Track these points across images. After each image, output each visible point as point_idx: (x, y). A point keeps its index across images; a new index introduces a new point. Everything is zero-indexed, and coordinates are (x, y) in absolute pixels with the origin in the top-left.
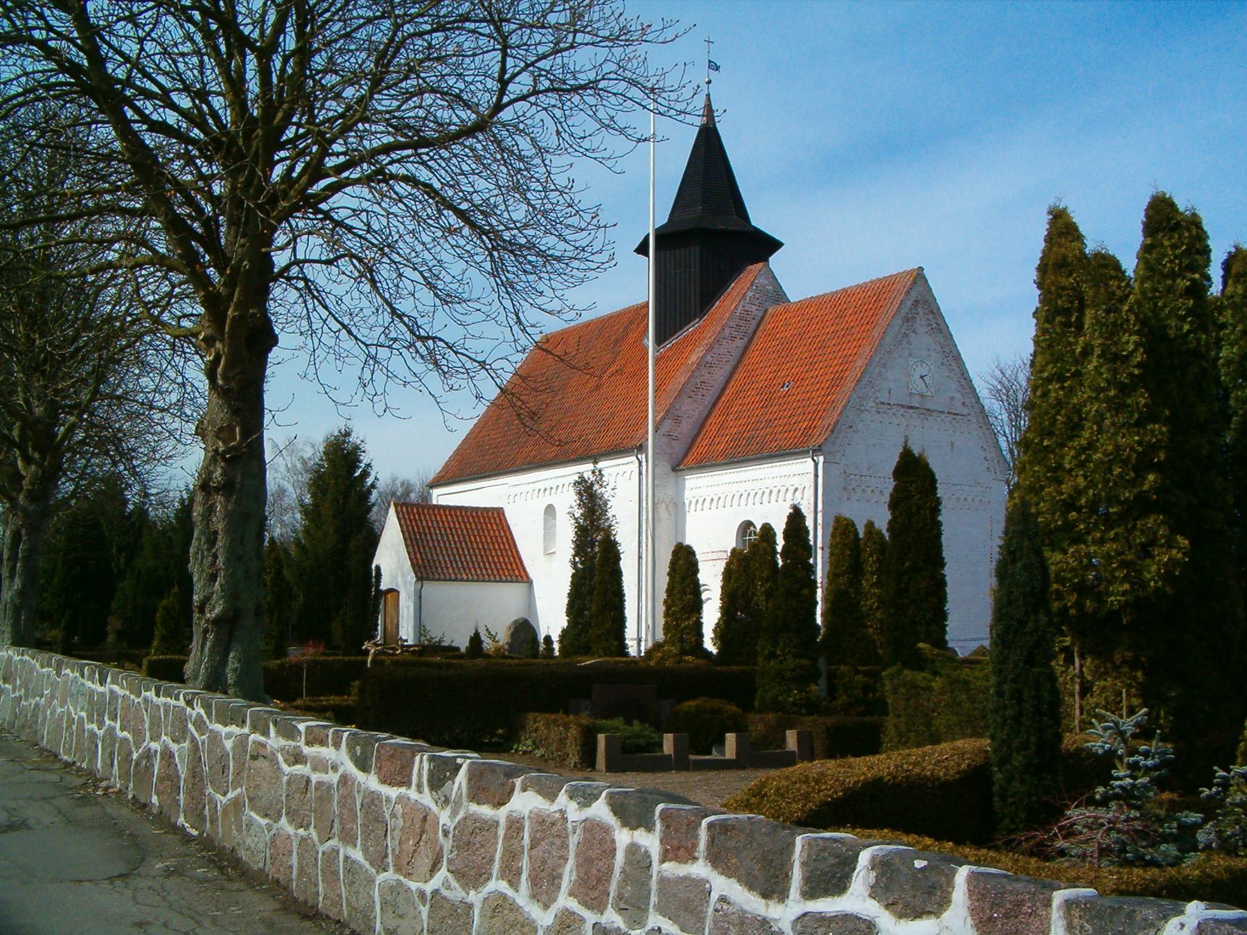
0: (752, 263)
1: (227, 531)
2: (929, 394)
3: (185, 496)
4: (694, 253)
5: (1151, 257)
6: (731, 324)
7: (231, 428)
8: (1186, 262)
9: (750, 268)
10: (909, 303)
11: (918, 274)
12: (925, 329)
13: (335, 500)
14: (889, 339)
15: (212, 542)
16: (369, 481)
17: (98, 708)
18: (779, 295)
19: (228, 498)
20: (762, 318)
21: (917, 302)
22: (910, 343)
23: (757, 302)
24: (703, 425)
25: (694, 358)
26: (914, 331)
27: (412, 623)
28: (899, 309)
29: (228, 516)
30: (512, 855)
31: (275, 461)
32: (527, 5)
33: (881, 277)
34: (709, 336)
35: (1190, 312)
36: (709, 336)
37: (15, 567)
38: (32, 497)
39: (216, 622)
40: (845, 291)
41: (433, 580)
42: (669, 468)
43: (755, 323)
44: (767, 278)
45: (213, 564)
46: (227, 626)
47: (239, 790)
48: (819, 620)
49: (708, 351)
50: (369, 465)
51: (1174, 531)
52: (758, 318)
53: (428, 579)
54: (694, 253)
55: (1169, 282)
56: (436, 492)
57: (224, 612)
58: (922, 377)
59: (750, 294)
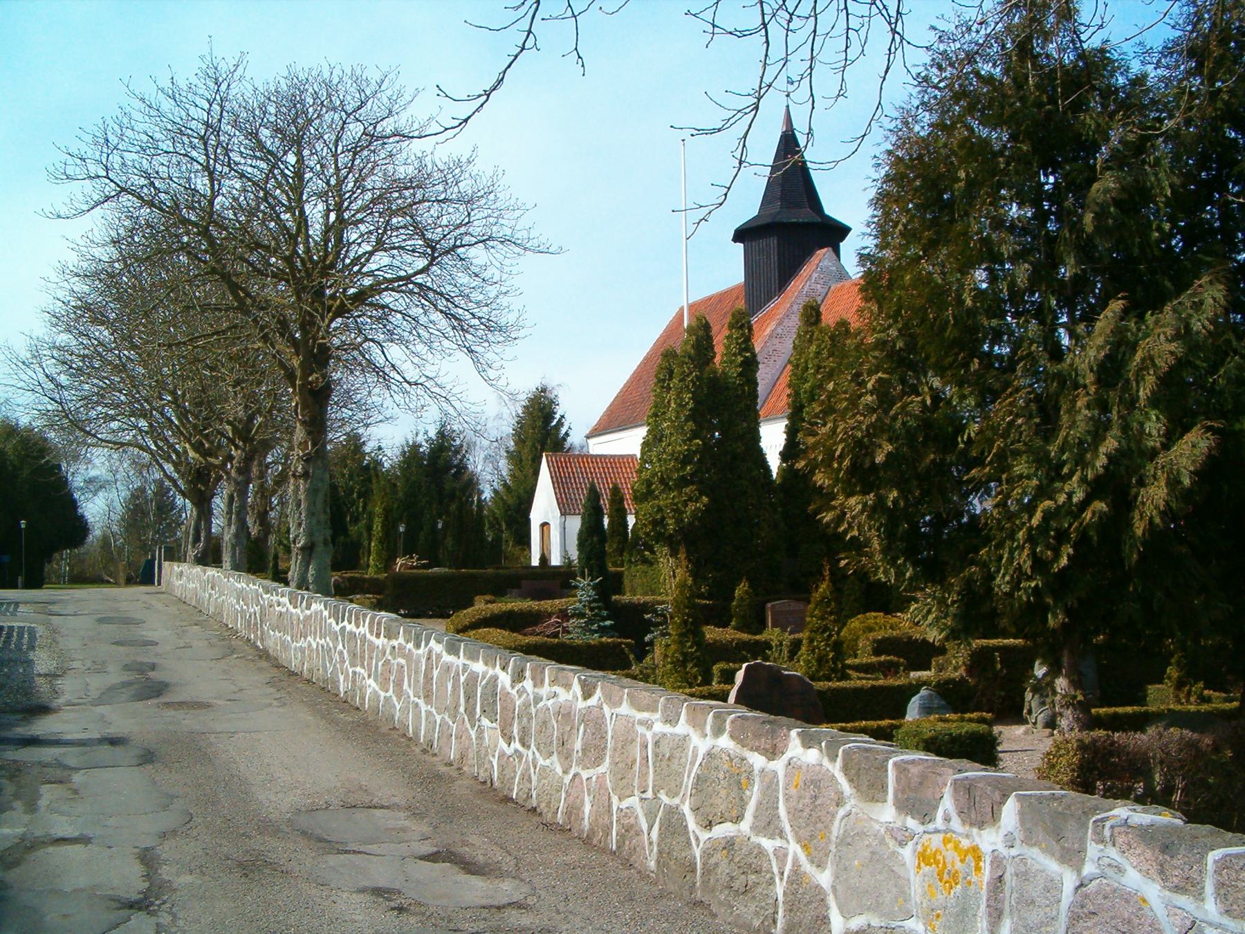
1: (306, 499)
3: (406, 449)
4: (773, 242)
6: (799, 301)
7: (306, 442)
8: (743, 346)
9: (819, 252)
15: (299, 505)
16: (563, 430)
17: (240, 595)
19: (306, 481)
23: (821, 282)
24: (775, 384)
25: (768, 331)
29: (307, 491)
34: (782, 311)
36: (782, 311)
37: (231, 518)
38: (240, 471)
39: (302, 549)
45: (300, 517)
46: (308, 550)
49: (779, 324)
50: (563, 417)
52: (823, 295)
53: (570, 514)
54: (773, 242)
56: (592, 441)
57: (305, 544)
59: (815, 275)
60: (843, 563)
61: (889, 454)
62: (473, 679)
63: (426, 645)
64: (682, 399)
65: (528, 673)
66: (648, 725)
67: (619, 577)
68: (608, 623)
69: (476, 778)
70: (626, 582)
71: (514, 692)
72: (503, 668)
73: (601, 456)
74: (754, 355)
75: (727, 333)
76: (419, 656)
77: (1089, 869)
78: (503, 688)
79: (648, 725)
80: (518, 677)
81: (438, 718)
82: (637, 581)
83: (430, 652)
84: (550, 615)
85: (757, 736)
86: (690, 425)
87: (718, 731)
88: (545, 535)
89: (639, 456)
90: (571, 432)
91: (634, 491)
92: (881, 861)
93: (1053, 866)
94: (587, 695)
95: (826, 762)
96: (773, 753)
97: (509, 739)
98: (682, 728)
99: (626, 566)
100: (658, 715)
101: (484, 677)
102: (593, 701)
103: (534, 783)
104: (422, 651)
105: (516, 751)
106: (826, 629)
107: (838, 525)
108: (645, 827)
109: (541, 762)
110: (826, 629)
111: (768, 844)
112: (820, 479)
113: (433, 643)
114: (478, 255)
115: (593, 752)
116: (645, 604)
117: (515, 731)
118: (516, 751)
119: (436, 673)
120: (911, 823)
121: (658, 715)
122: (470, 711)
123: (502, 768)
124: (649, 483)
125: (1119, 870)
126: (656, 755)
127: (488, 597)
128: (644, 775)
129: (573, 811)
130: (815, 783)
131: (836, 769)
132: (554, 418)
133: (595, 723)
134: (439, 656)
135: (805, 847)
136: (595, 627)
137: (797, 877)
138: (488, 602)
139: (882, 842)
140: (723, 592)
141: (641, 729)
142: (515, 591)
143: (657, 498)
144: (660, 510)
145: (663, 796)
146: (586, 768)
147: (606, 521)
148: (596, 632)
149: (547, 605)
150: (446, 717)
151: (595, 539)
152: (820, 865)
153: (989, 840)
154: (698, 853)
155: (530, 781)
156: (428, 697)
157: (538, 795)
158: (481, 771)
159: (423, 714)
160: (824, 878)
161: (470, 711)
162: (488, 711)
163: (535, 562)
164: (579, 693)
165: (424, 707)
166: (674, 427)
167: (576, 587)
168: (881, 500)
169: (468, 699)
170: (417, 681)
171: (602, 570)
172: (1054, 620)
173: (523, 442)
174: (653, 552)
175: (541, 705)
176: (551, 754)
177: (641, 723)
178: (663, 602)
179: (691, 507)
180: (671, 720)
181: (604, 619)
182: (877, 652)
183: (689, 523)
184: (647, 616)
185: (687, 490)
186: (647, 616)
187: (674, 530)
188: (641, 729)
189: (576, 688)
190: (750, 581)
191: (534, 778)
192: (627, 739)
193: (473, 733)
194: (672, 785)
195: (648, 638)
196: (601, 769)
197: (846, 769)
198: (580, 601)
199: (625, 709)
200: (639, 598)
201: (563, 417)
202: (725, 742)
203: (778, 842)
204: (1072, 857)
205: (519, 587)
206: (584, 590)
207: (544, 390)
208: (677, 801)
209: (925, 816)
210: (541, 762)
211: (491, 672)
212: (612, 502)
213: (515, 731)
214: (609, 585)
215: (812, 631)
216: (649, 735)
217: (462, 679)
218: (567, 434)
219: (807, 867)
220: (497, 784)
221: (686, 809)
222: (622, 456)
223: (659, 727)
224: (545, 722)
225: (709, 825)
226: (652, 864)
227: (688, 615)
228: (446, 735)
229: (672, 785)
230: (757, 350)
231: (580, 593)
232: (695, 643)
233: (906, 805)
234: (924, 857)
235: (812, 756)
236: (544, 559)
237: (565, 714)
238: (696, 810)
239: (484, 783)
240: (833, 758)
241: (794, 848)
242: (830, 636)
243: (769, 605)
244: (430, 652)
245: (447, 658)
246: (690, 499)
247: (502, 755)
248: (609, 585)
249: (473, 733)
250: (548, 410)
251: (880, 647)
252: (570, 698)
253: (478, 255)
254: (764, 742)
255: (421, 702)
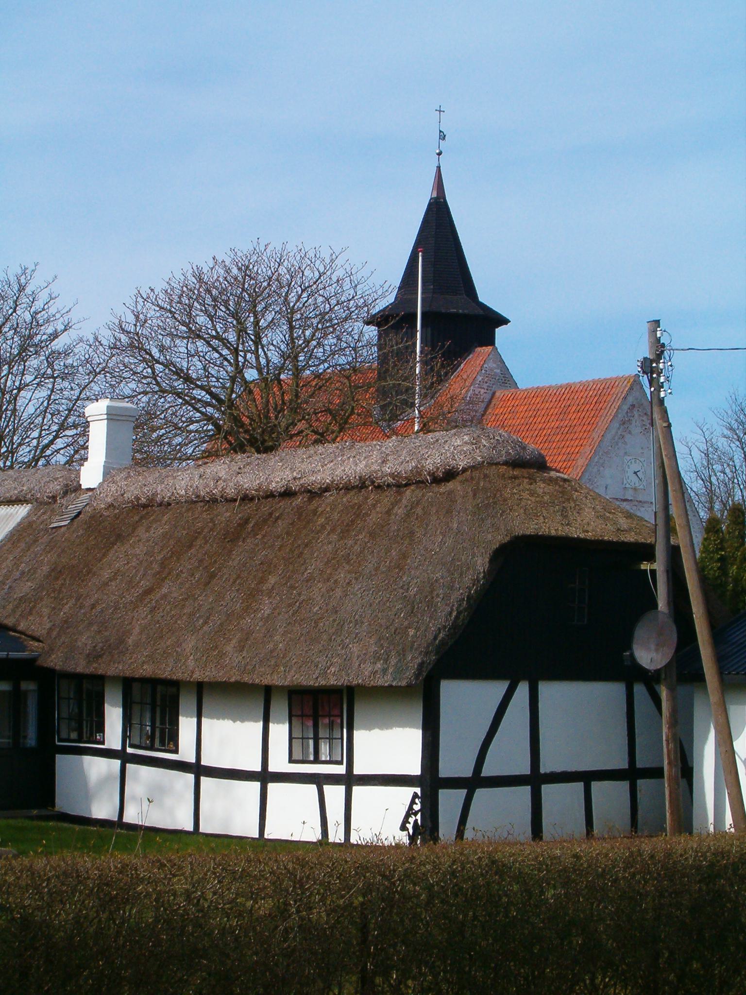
0: (481, 345)
2: (641, 487)
5: (706, 543)
9: (479, 349)
10: (625, 408)
11: (634, 381)
12: (639, 430)
14: (609, 436)
18: (506, 379)
20: (490, 402)
21: (633, 406)
22: (625, 443)
23: (485, 386)
26: (630, 433)
28: (616, 416)
33: (602, 378)
35: (719, 568)
40: (569, 386)
43: (483, 405)
44: (494, 362)
48: (417, 372)
55: (712, 555)
58: (635, 473)
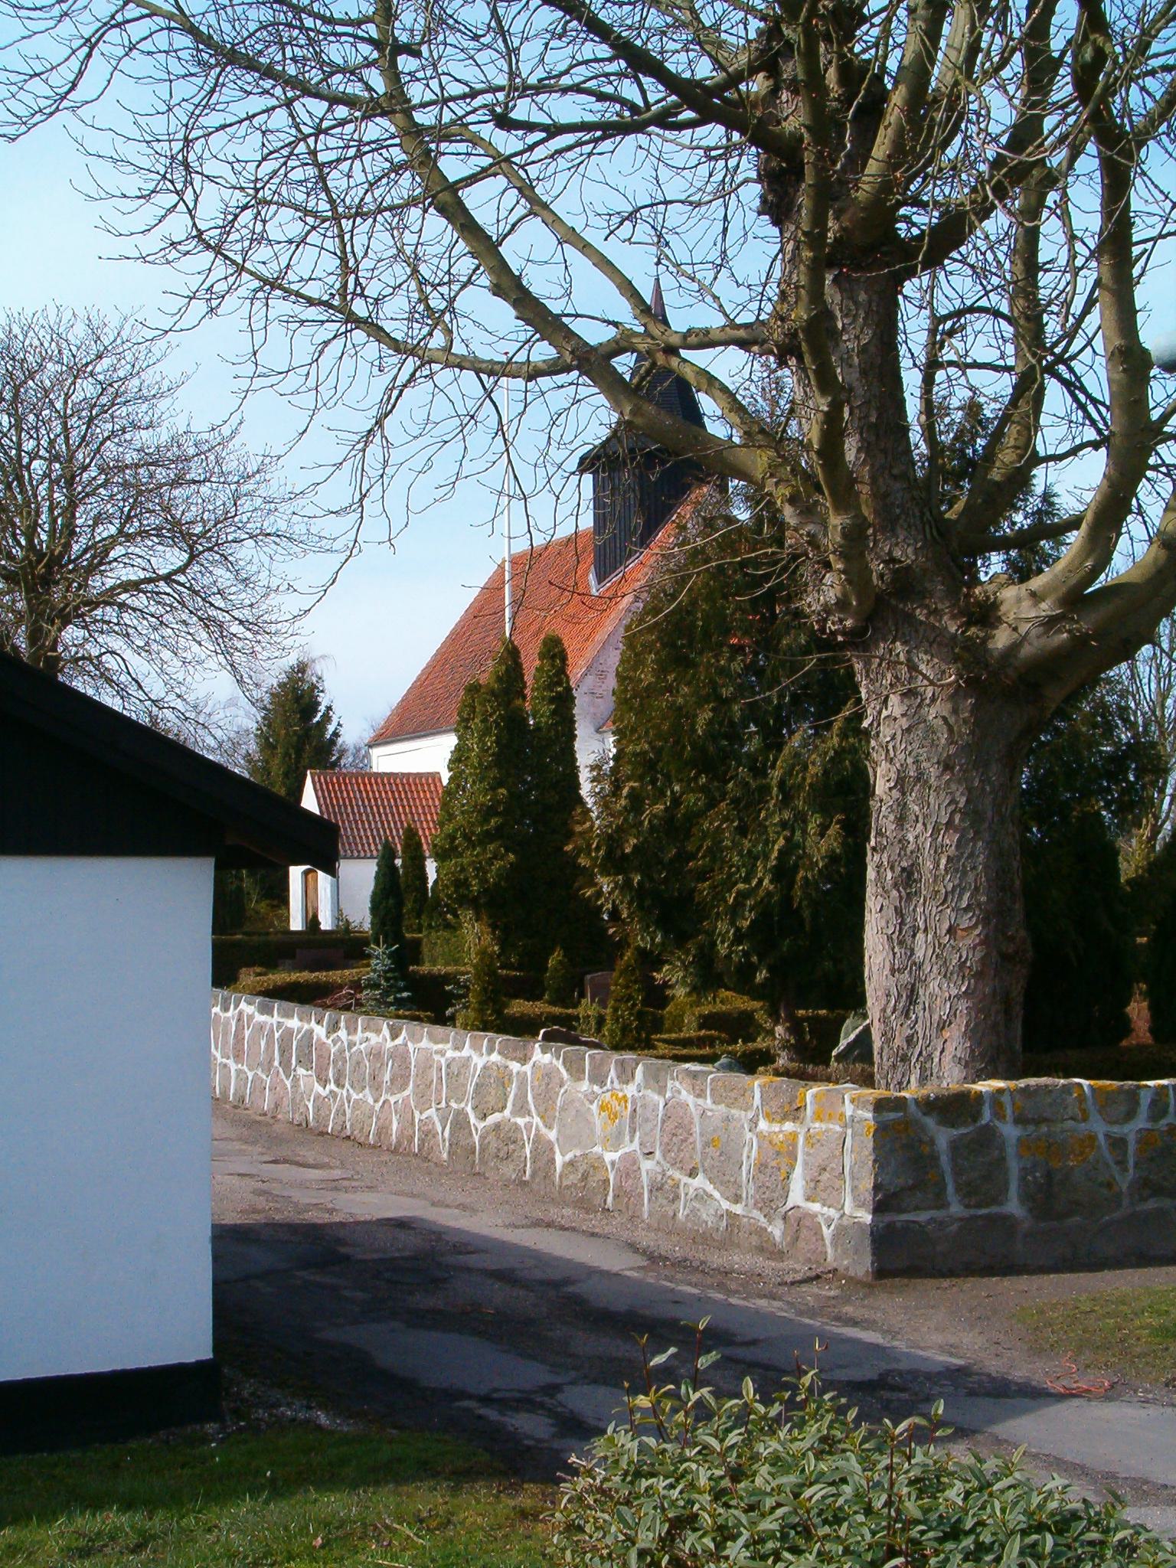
13: (287, 754)
16: (331, 728)
27: (329, 906)
30: (521, 1097)
31: (990, 356)
32: (6, 417)
41: (352, 857)
42: (593, 730)
47: (423, 1117)
50: (329, 708)
51: (507, 850)
56: (375, 752)
60: (611, 931)
61: (635, 846)
62: (289, 1033)
63: (236, 1008)
64: (485, 744)
65: (342, 1024)
66: (442, 1053)
67: (417, 944)
68: (405, 994)
69: (292, 1123)
70: (425, 950)
71: (329, 1041)
72: (318, 1023)
73: (390, 775)
74: (569, 689)
75: (538, 663)
76: (227, 1021)
77: (668, 1095)
78: (319, 1039)
79: (442, 1053)
80: (334, 1027)
81: (250, 1075)
82: (438, 949)
83: (241, 1013)
84: (341, 987)
85: (515, 1050)
86: (494, 772)
87: (490, 1051)
88: (310, 887)
89: (445, 777)
90: (342, 731)
91: (435, 846)
92: (582, 1116)
93: (656, 1097)
94: (394, 1037)
95: (554, 1061)
96: (524, 1060)
97: (324, 1083)
98: (467, 1051)
99: (425, 933)
100: (449, 1045)
101: (299, 1032)
102: (399, 1041)
103: (348, 1116)
104: (232, 1013)
105: (331, 1092)
106: (630, 998)
107: (598, 899)
108: (439, 1129)
109: (355, 1096)
110: (630, 998)
111: (521, 1121)
112: (583, 861)
113: (243, 1005)
114: (245, 552)
115: (400, 1081)
116: (447, 975)
117: (331, 1075)
118: (331, 1092)
119: (247, 1033)
120: (596, 1088)
121: (449, 1045)
122: (285, 1064)
123: (317, 1109)
124: (452, 838)
125: (679, 1092)
126: (448, 1074)
127: (258, 970)
128: (439, 1091)
129: (383, 1130)
130: (548, 1076)
131: (559, 1064)
132: (316, 711)
133: (401, 1057)
134: (251, 1017)
135: (542, 1118)
136: (391, 999)
137: (538, 1139)
138: (260, 974)
139: (583, 1104)
140: (535, 961)
141: (436, 1057)
142: (288, 962)
143: (460, 855)
144: (463, 870)
145: (454, 1105)
146: (393, 1094)
147: (398, 862)
148: (391, 1004)
149: (335, 976)
150: (259, 1072)
151: (391, 901)
152: (550, 1128)
153: (630, 1090)
154: (476, 1138)
155: (344, 1114)
156: (238, 1058)
157: (352, 1125)
158: (297, 1116)
159: (233, 1073)
160: (552, 1135)
161: (285, 1064)
162: (304, 1060)
163: (296, 924)
164: (388, 1037)
165: (233, 1066)
166: (476, 775)
167: (369, 956)
168: (628, 883)
169: (282, 1052)
170: (225, 1043)
171: (398, 937)
172: (761, 976)
173: (273, 747)
174: (456, 916)
175: (354, 1049)
176: (364, 1088)
177: (437, 1052)
178: (463, 974)
179: (498, 864)
180: (458, 1047)
181: (401, 990)
182: (701, 1027)
183: (495, 884)
184: (448, 988)
185: (491, 847)
186: (448, 988)
187: (479, 892)
188: (436, 1057)
189: (386, 1031)
190: (566, 949)
191: (348, 1112)
192: (426, 1064)
193: (288, 1083)
194: (456, 1090)
195: (449, 1012)
196: (406, 1093)
197: (564, 1063)
198: (375, 971)
199: (425, 1043)
200: (440, 968)
201: (329, 708)
202: (495, 1057)
203: (527, 1119)
204: (662, 1091)
205: (293, 957)
206: (380, 958)
207: (302, 668)
208: (462, 1105)
209: (602, 1084)
210: (355, 1096)
211: (306, 1027)
212: (406, 847)
213: (331, 1075)
214: (406, 955)
215: (616, 1000)
216: (443, 1061)
217: (277, 1035)
218: (336, 734)
219: (544, 1130)
220: (312, 1124)
221: (469, 1109)
222: (419, 775)
223: (450, 1054)
224: (358, 1063)
225: (485, 1116)
226: (445, 1156)
227: (489, 983)
228: (258, 1087)
229: (459, 1096)
230: (572, 684)
231: (374, 962)
232: (494, 1011)
233: (593, 1080)
234: (602, 1108)
235: (547, 1058)
236: (313, 922)
237: (376, 1054)
238: (475, 1108)
239: (300, 1125)
240: (558, 1059)
241: (537, 1120)
242: (634, 1005)
243: (588, 977)
244: (241, 1013)
245: (260, 1018)
246: (495, 857)
247: (318, 1097)
248: (406, 955)
249: (288, 1083)
250: (306, 700)
251: (706, 1022)
252: (380, 1040)
253: (245, 552)
254: (519, 1054)
255: (231, 1063)
